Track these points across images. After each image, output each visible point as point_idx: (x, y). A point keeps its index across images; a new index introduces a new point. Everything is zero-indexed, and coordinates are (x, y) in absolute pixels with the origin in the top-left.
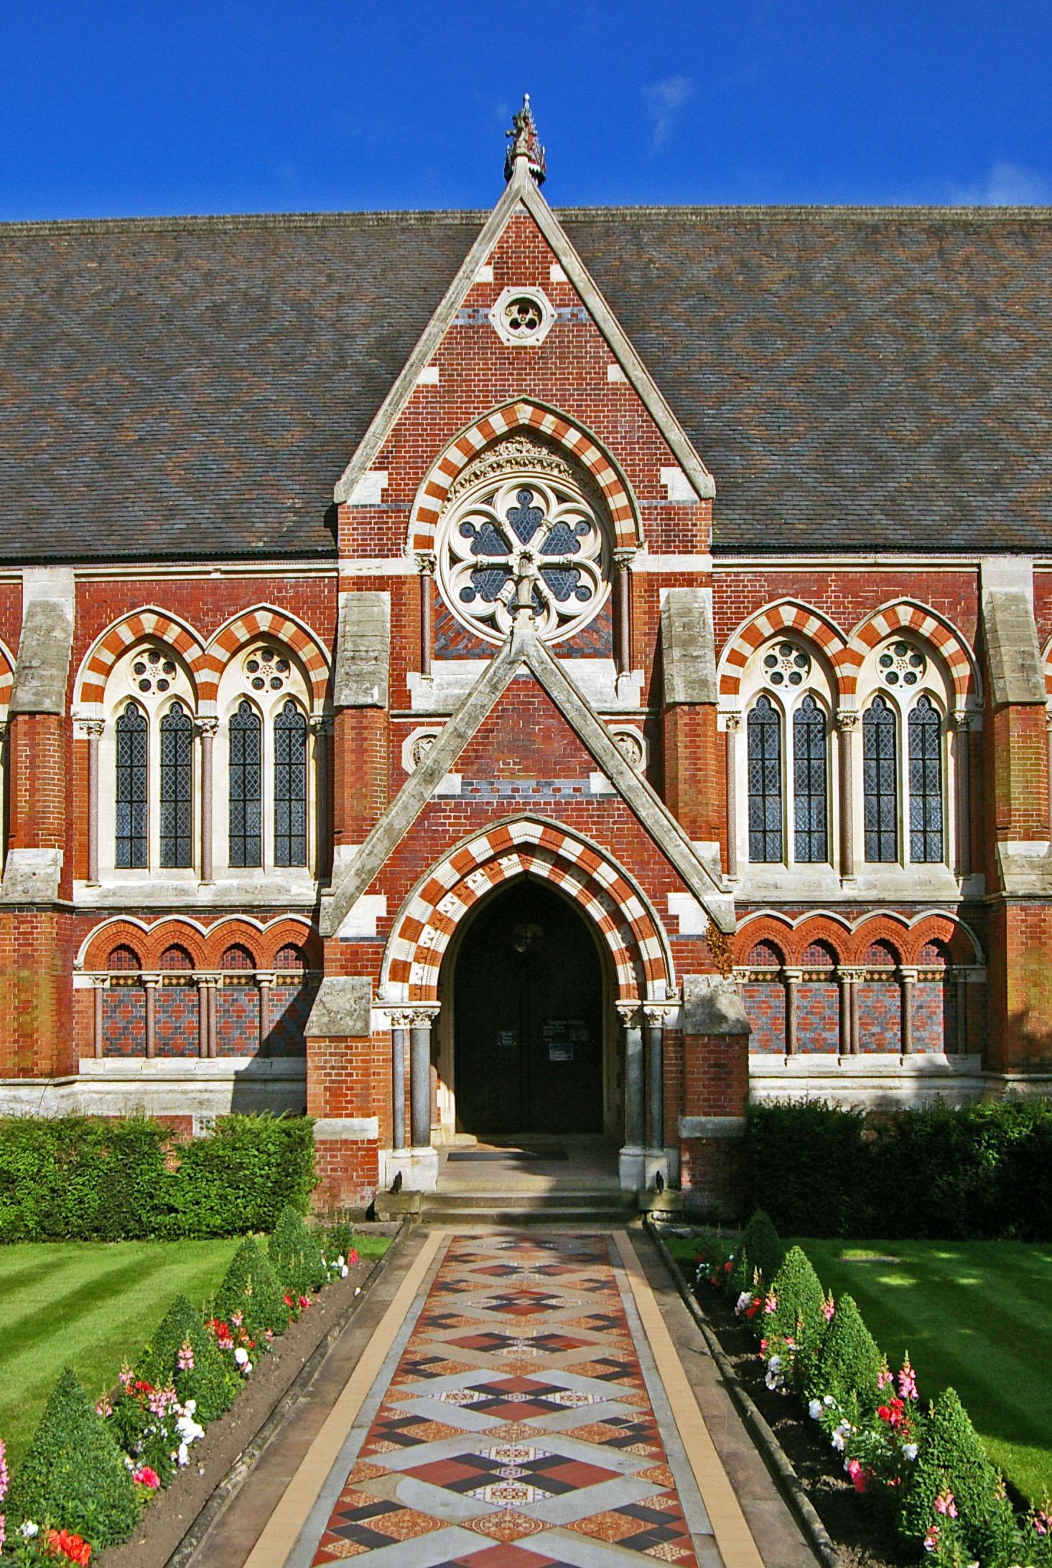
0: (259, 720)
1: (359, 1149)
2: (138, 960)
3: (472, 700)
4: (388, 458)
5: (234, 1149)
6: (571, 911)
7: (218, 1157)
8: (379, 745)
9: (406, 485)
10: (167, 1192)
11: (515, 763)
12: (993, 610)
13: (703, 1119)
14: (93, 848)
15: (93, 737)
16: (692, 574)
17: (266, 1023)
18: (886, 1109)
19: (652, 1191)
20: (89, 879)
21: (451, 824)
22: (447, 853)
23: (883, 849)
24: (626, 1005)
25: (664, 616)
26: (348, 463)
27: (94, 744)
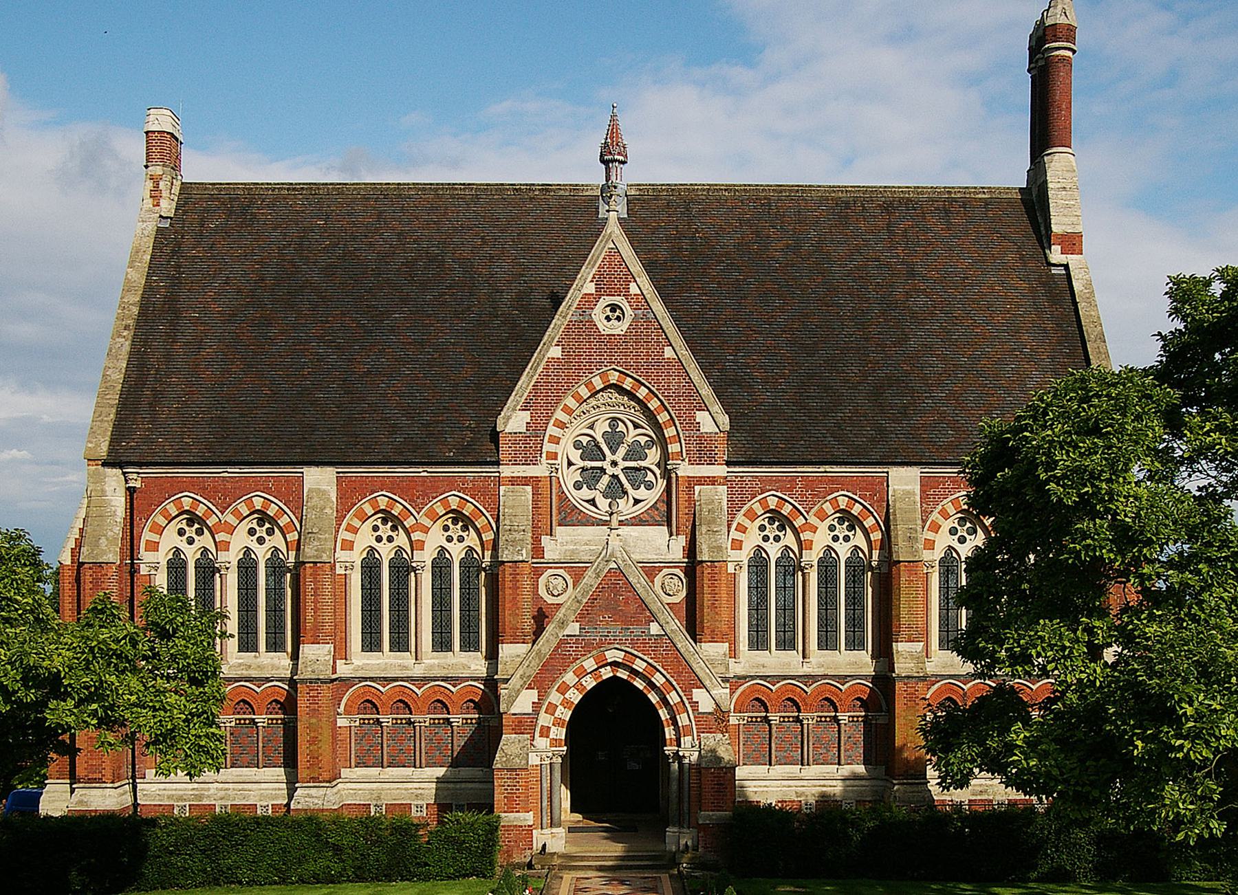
0: (184, 564)
1: (523, 830)
4: (529, 403)
5: (460, 832)
7: (452, 837)
8: (526, 583)
9: (541, 420)
10: (424, 856)
11: (609, 617)
12: (894, 501)
13: (711, 813)
17: (455, 748)
18: (825, 801)
19: (683, 852)
20: (346, 659)
21: (573, 651)
22: (571, 667)
23: (828, 641)
24: (669, 749)
25: (697, 504)
26: (505, 404)
27: (348, 576)
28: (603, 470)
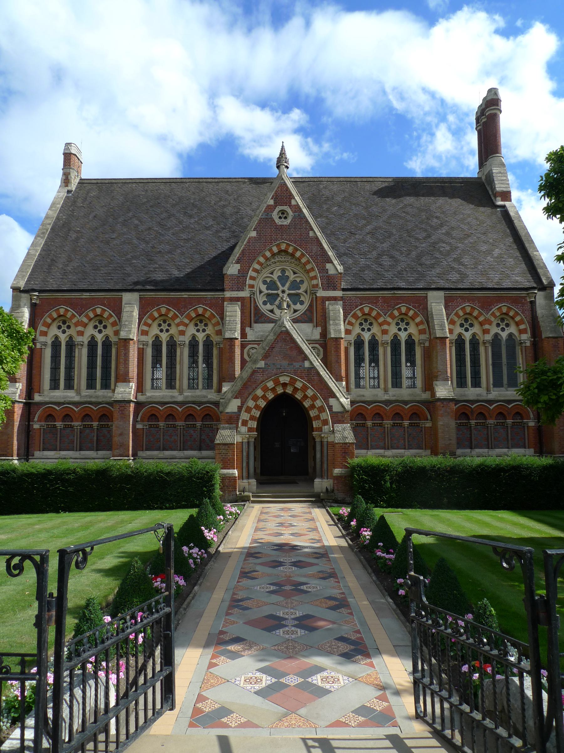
1: (232, 480)
2: (158, 419)
3: (268, 338)
6: (298, 405)
14: (144, 383)
15: (145, 347)
16: (336, 297)
27: (145, 349)
28: (278, 295)
